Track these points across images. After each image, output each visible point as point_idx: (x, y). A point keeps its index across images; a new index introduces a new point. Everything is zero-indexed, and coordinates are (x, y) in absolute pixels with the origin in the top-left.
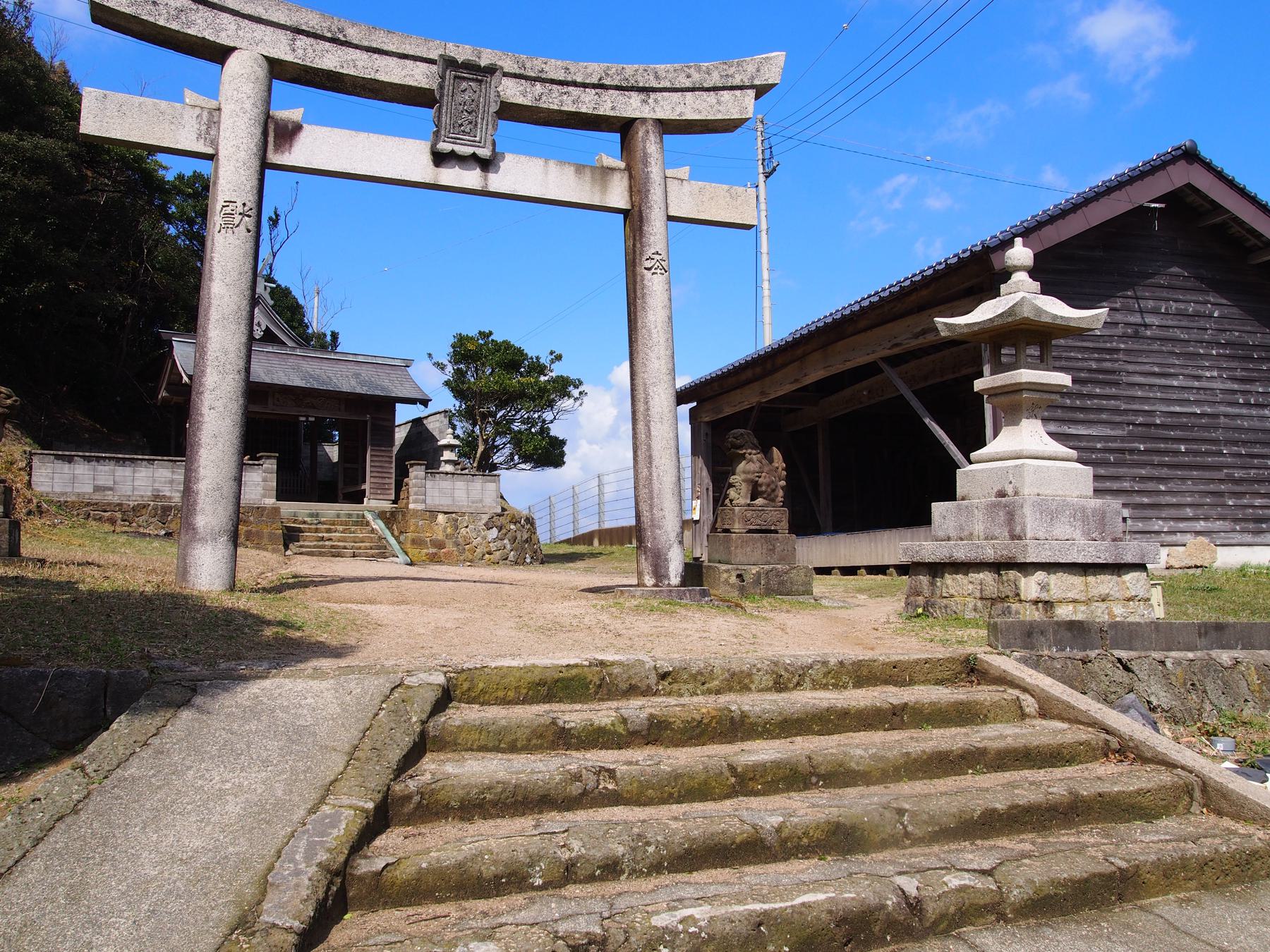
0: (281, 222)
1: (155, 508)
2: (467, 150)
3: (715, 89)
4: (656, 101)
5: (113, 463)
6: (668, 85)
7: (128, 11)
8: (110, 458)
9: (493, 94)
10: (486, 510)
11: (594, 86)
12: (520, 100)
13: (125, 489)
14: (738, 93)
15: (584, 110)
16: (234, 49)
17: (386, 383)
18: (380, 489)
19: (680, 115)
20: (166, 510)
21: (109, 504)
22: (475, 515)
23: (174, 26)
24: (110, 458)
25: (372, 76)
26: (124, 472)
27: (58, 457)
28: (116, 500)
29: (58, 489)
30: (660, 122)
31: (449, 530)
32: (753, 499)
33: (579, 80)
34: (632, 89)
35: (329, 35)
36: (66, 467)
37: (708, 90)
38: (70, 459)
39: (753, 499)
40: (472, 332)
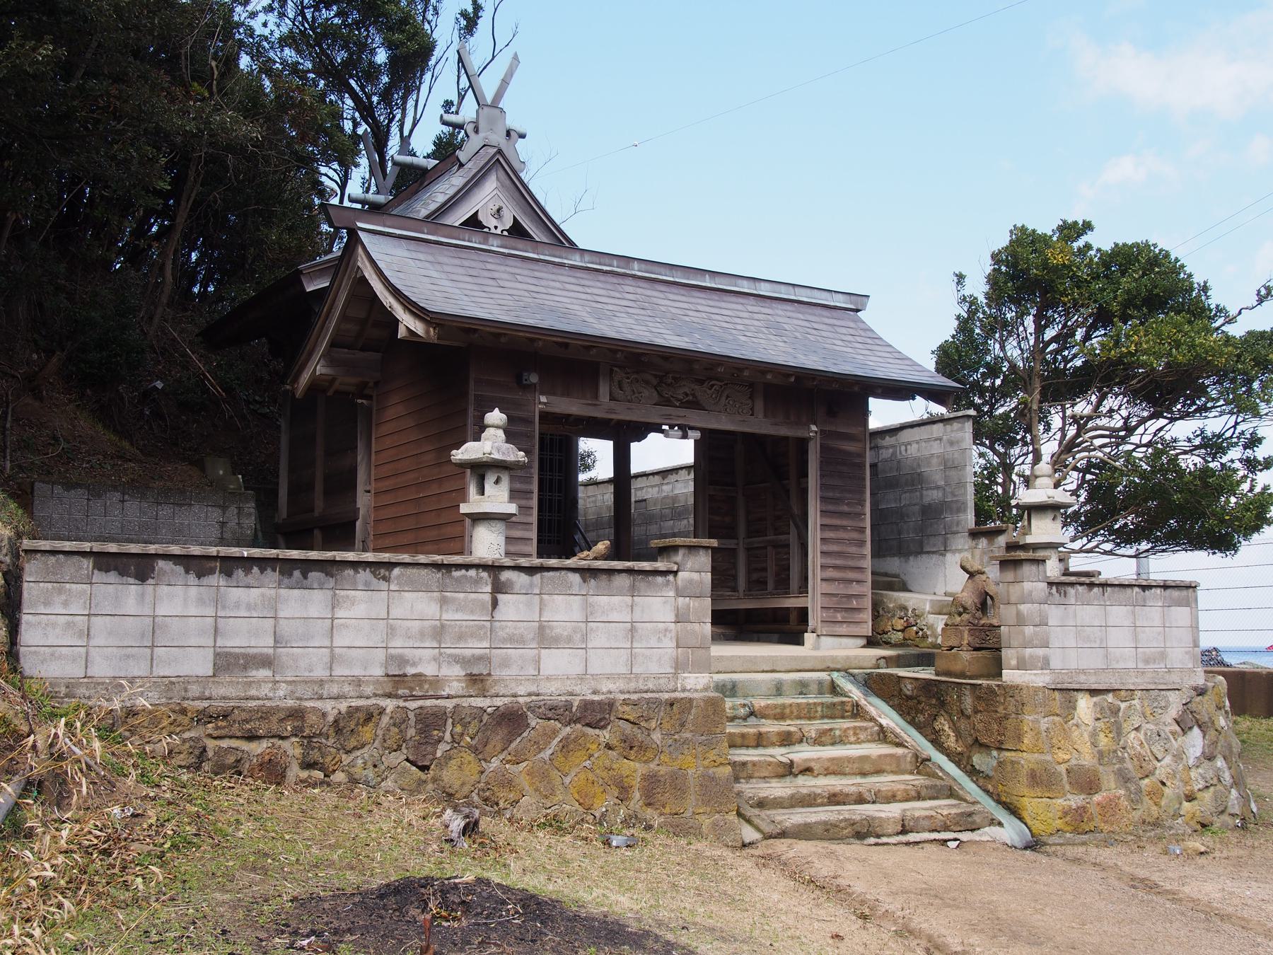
0: (483, 24)
1: (400, 722)
5: (272, 576)
8: (263, 563)
10: (1175, 678)
13: (308, 662)
17: (840, 347)
18: (842, 609)
20: (430, 722)
21: (265, 714)
22: (1154, 693)
24: (263, 563)
26: (303, 605)
27: (104, 562)
28: (281, 697)
29: (102, 669)
31: (1104, 741)
36: (130, 595)
38: (140, 568)
40: (1046, 226)
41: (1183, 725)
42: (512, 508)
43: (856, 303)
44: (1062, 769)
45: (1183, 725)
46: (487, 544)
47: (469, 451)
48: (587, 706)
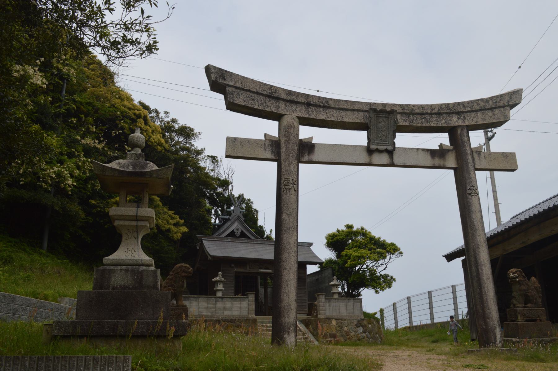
2: (383, 148)
3: (491, 109)
4: (464, 117)
6: (469, 109)
7: (243, 104)
9: (392, 122)
11: (436, 114)
12: (404, 124)
14: (502, 109)
15: (432, 125)
16: (285, 114)
19: (476, 122)
23: (261, 108)
25: (341, 120)
30: (467, 126)
32: (525, 304)
33: (429, 112)
34: (452, 113)
35: (322, 105)
37: (488, 109)
39: (525, 304)
41: (358, 326)
42: (223, 289)
43: (310, 244)
44: (328, 334)
45: (358, 326)
46: (219, 294)
47: (332, 283)
48: (231, 319)
